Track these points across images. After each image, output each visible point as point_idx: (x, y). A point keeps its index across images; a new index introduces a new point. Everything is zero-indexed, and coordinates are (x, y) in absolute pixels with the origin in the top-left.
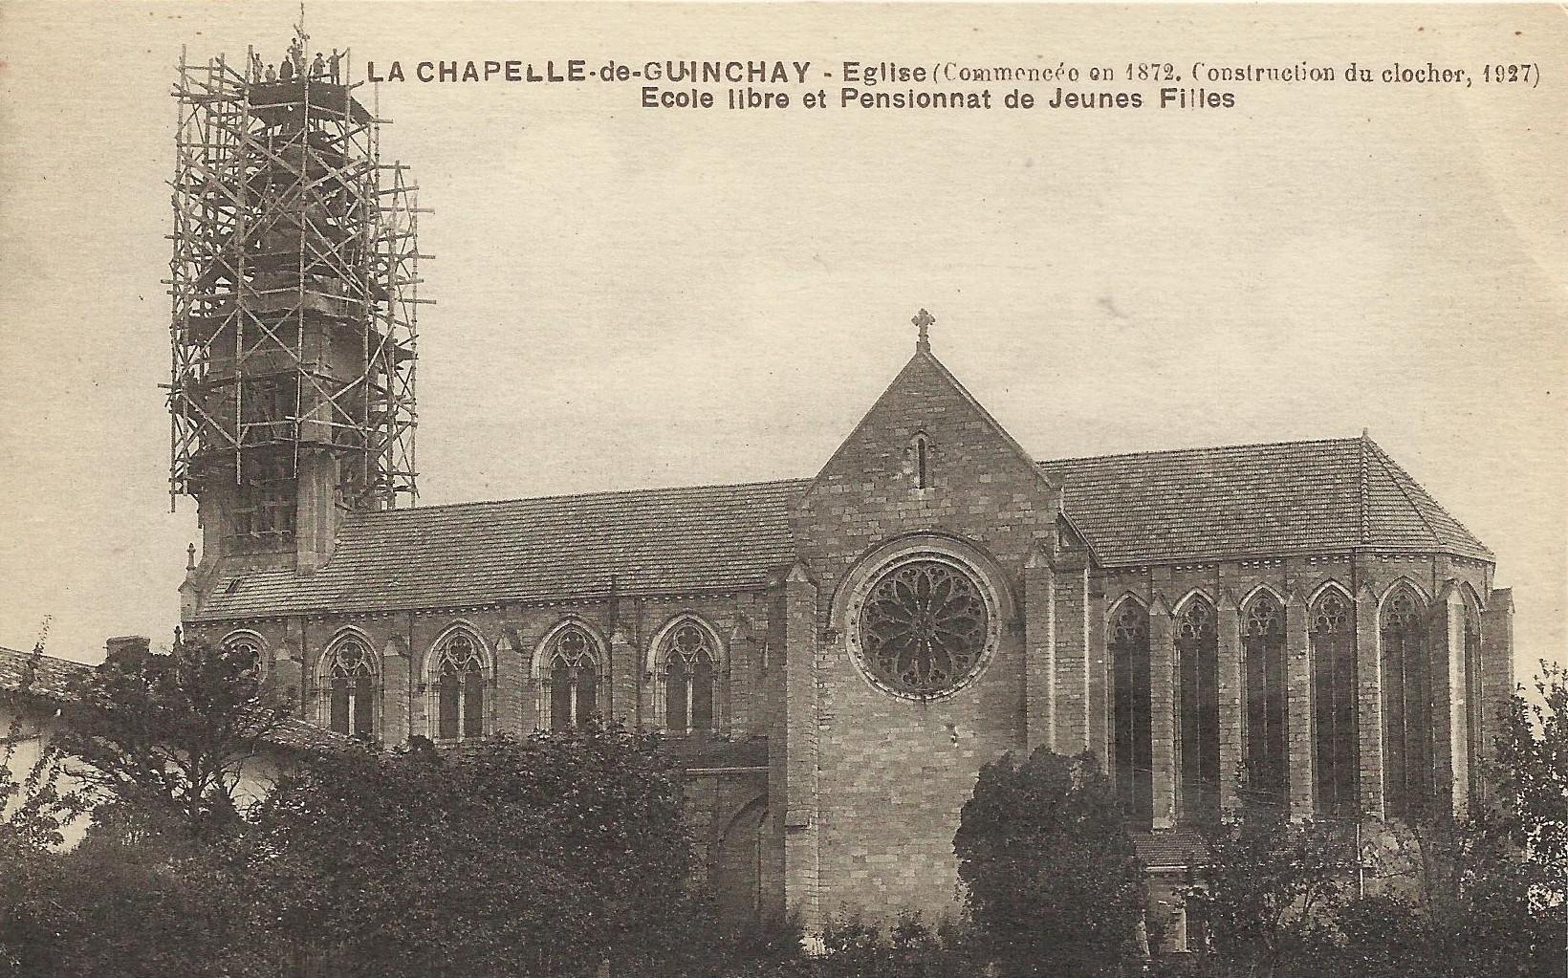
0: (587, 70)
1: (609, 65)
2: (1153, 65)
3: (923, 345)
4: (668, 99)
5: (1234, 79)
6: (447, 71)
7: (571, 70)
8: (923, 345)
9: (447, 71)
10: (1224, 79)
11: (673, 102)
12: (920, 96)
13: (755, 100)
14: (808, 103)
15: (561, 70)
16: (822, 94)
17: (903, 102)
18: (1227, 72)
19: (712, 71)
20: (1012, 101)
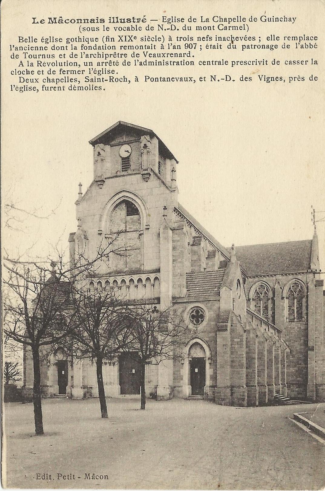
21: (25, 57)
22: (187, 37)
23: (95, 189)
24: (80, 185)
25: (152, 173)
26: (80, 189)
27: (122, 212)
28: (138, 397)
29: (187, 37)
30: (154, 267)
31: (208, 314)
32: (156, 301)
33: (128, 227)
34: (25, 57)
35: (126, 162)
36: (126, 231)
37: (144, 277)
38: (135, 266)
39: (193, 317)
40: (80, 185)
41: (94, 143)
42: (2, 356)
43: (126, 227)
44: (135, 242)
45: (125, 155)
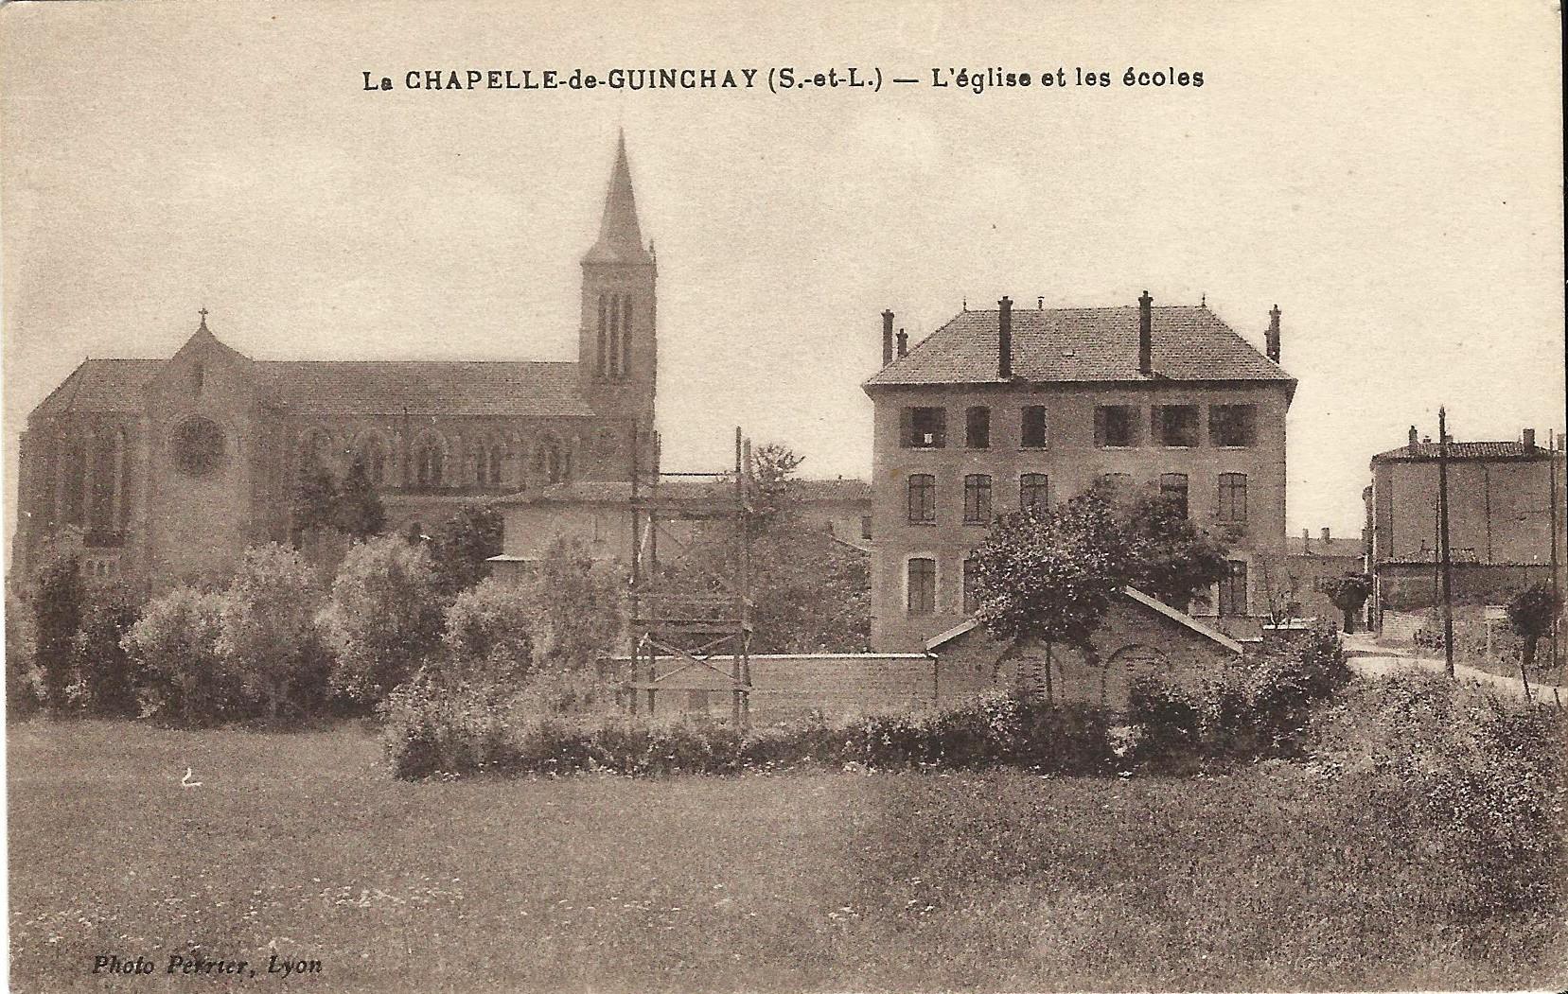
0: (556, 80)
1: (576, 74)
2: (862, 85)
3: (203, 324)
4: (1144, 80)
5: (1005, 85)
6: (433, 80)
7: (547, 80)
8: (203, 324)
9: (433, 80)
10: (652, 86)
11: (1148, 82)
12: (1163, 82)
13: (977, 81)
14: (589, 84)
15: (537, 78)
16: (1060, 74)
17: (782, 76)
18: (636, 83)
19: (667, 78)
20: (575, 82)
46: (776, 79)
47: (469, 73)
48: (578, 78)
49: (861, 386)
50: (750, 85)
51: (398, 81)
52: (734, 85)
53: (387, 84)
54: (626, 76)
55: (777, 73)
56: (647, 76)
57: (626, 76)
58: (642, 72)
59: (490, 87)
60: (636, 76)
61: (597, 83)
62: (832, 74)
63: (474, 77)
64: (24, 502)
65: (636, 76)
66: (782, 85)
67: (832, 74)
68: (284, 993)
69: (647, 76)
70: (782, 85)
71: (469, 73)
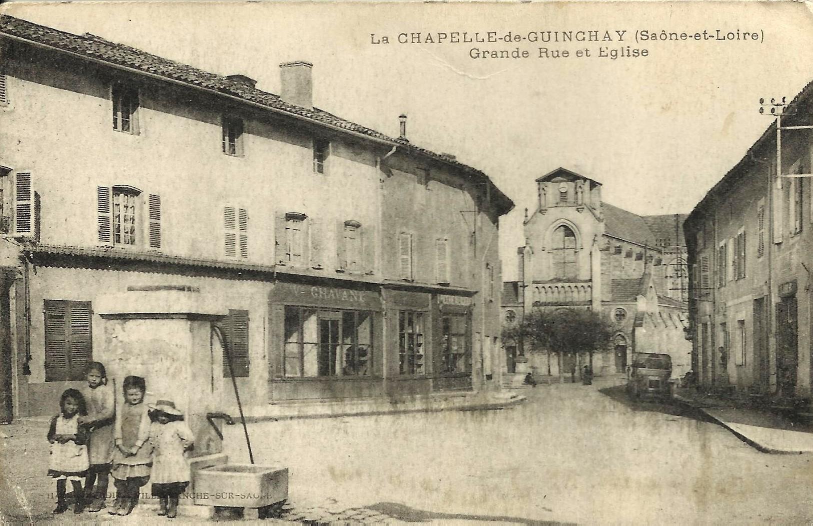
5: (632, 55)
21: (556, 35)
22: (735, 32)
23: (539, 214)
24: (526, 210)
25: (585, 207)
26: (526, 213)
27: (561, 233)
28: (610, 402)
29: (735, 32)
30: (588, 278)
31: (630, 314)
32: (589, 304)
33: (566, 245)
34: (556, 35)
35: (564, 196)
36: (564, 248)
37: (579, 285)
38: (571, 275)
39: (623, 315)
40: (526, 210)
41: (539, 181)
42: (135, 316)
43: (564, 245)
44: (571, 258)
45: (563, 190)
46: (639, 36)
47: (439, 34)
48: (510, 36)
49: (286, 470)
50: (621, 40)
51: (393, 38)
52: (610, 40)
53: (386, 40)
54: (539, 35)
55: (639, 32)
56: (553, 35)
57: (539, 35)
58: (542, 33)
59: (452, 42)
60: (546, 35)
61: (522, 39)
62: (705, 33)
63: (442, 36)
64: (503, 196)
65: (546, 35)
66: (642, 39)
67: (705, 33)
68: (811, 415)
69: (553, 35)
70: (642, 39)
71: (439, 34)
